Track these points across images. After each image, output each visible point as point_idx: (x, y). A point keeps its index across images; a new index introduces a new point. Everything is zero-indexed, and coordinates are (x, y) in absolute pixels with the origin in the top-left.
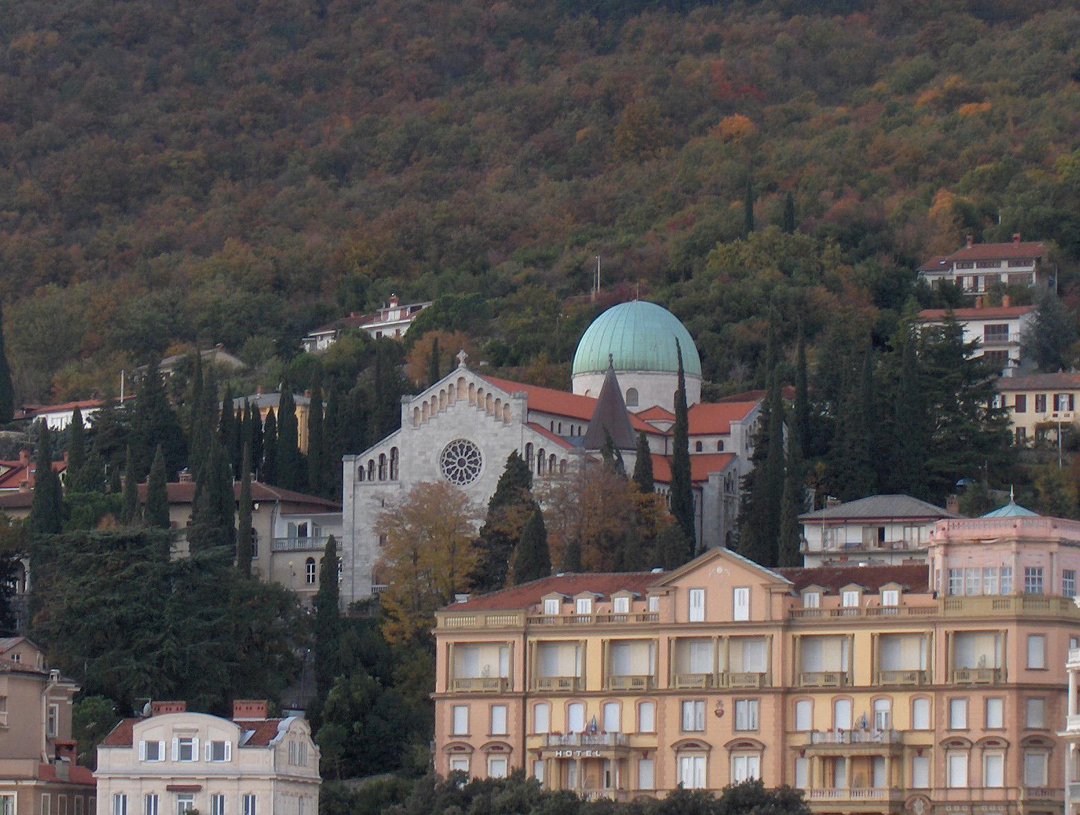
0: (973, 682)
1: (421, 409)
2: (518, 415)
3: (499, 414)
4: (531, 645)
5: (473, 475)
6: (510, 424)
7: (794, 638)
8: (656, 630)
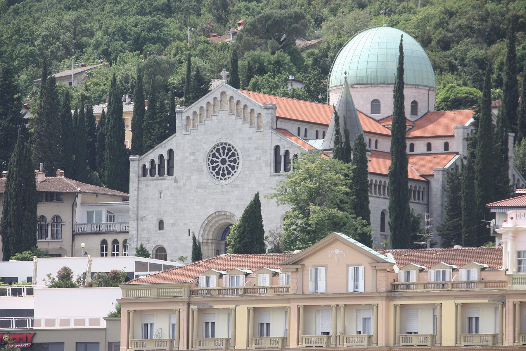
0: (314, 346)
1: (191, 117)
2: (268, 122)
3: (253, 121)
4: (193, 312)
5: (233, 172)
6: (262, 130)
7: (395, 307)
8: (288, 300)
